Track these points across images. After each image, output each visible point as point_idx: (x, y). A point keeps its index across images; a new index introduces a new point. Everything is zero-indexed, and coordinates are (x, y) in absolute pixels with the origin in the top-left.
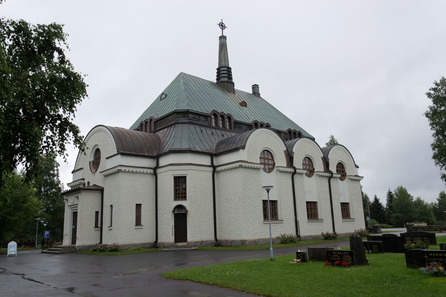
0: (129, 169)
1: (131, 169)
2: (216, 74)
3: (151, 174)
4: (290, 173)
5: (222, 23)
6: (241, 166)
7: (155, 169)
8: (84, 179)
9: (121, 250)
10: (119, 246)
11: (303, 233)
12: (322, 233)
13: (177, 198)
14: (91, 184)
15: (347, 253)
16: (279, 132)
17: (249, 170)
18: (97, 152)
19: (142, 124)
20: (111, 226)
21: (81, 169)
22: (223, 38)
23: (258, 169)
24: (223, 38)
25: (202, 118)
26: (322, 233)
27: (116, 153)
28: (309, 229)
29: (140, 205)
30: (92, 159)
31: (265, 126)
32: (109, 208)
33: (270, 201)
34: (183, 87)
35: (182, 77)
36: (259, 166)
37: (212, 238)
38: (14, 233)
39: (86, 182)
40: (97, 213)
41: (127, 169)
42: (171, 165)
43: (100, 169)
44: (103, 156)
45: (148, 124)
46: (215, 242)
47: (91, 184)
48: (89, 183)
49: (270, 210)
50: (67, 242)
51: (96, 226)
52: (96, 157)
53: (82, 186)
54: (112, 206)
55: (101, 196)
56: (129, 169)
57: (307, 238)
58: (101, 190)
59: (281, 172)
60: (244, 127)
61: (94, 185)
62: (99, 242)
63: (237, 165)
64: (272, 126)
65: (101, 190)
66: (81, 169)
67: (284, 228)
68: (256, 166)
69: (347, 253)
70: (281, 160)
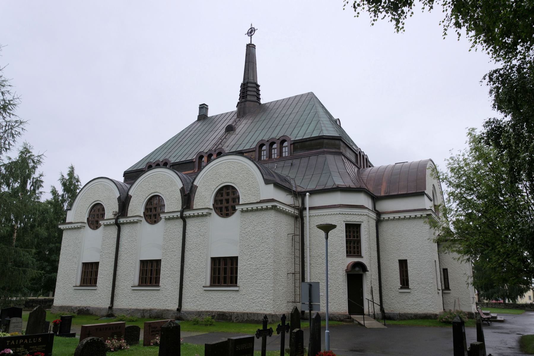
0: (416, 214)
1: (407, 215)
2: (261, 93)
5: (255, 31)
6: (274, 208)
9: (92, 314)
11: (187, 307)
13: (349, 253)
17: (74, 231)
22: (250, 49)
24: (250, 49)
31: (154, 166)
35: (311, 98)
37: (175, 307)
41: (402, 215)
49: (224, 272)
56: (389, 216)
59: (247, 211)
62: (176, 307)
63: (270, 205)
67: (161, 299)
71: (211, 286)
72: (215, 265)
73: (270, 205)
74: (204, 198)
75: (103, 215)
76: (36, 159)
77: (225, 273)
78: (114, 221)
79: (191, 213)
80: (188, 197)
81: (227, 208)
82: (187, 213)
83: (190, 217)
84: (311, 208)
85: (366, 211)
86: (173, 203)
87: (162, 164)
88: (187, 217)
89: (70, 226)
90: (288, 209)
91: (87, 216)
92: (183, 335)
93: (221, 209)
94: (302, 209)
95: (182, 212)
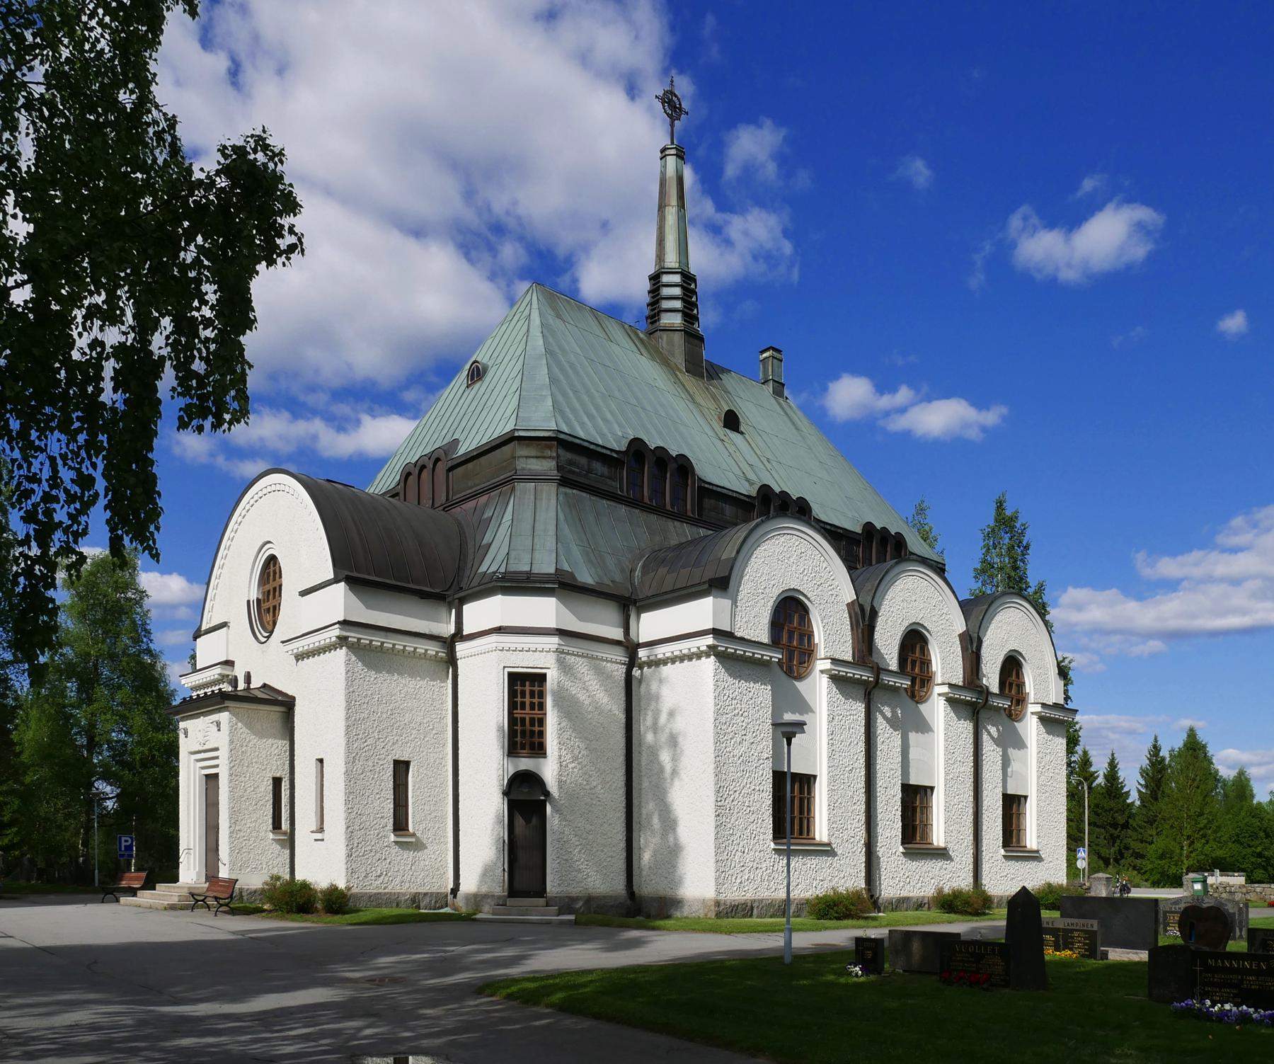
3: (435, 659)
4: (865, 683)
7: (449, 644)
8: (229, 663)
10: (355, 896)
11: (889, 889)
12: (940, 891)
13: (513, 749)
14: (255, 684)
15: (993, 950)
16: (835, 535)
18: (271, 570)
19: (409, 474)
20: (321, 830)
21: (224, 625)
23: (763, 664)
25: (598, 467)
26: (940, 891)
27: (331, 576)
28: (904, 878)
29: (407, 764)
30: (254, 594)
32: (313, 765)
33: (795, 775)
34: (541, 342)
36: (767, 655)
38: (157, 321)
39: (239, 672)
40: (277, 782)
42: (499, 630)
43: (281, 632)
44: (291, 584)
45: (425, 474)
46: (629, 902)
47: (255, 684)
48: (248, 678)
50: (190, 871)
51: (277, 825)
52: (267, 587)
53: (227, 688)
54: (321, 761)
55: (635, 888)
57: (900, 904)
58: (286, 705)
60: (729, 510)
61: (265, 686)
64: (818, 511)
65: (286, 705)
66: (224, 625)
68: (759, 653)
69: (993, 950)
70: (831, 636)
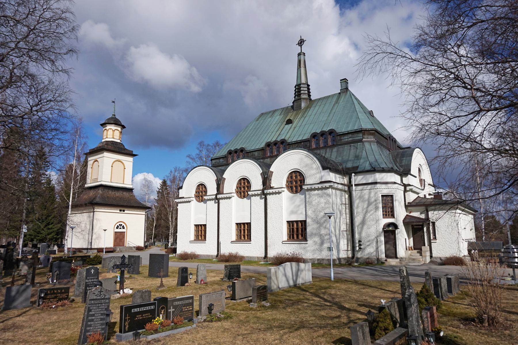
71: (288, 240)
72: (290, 226)
73: (327, 185)
74: (230, 185)
75: (206, 192)
76: (420, 32)
77: (244, 233)
78: (215, 196)
79: (271, 191)
80: (220, 183)
81: (296, 187)
82: (219, 196)
83: (222, 199)
84: (355, 185)
85: (397, 185)
86: (257, 184)
87: (233, 152)
88: (267, 194)
89: (274, 191)
90: (340, 187)
91: (194, 192)
92: (148, 274)
93: (292, 188)
94: (350, 185)
95: (263, 191)
